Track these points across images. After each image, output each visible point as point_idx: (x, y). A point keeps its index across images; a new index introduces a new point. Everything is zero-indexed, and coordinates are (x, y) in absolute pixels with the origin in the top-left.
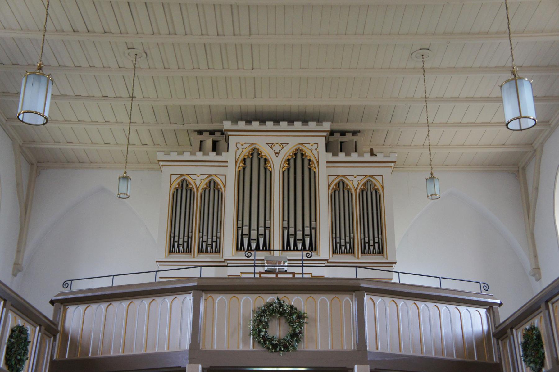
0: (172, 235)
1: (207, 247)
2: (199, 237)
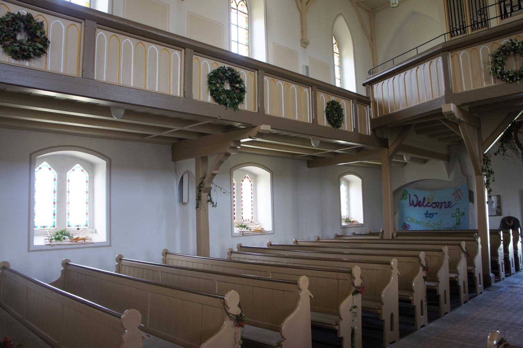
0: (451, 24)
1: (478, 25)
2: (471, 20)
